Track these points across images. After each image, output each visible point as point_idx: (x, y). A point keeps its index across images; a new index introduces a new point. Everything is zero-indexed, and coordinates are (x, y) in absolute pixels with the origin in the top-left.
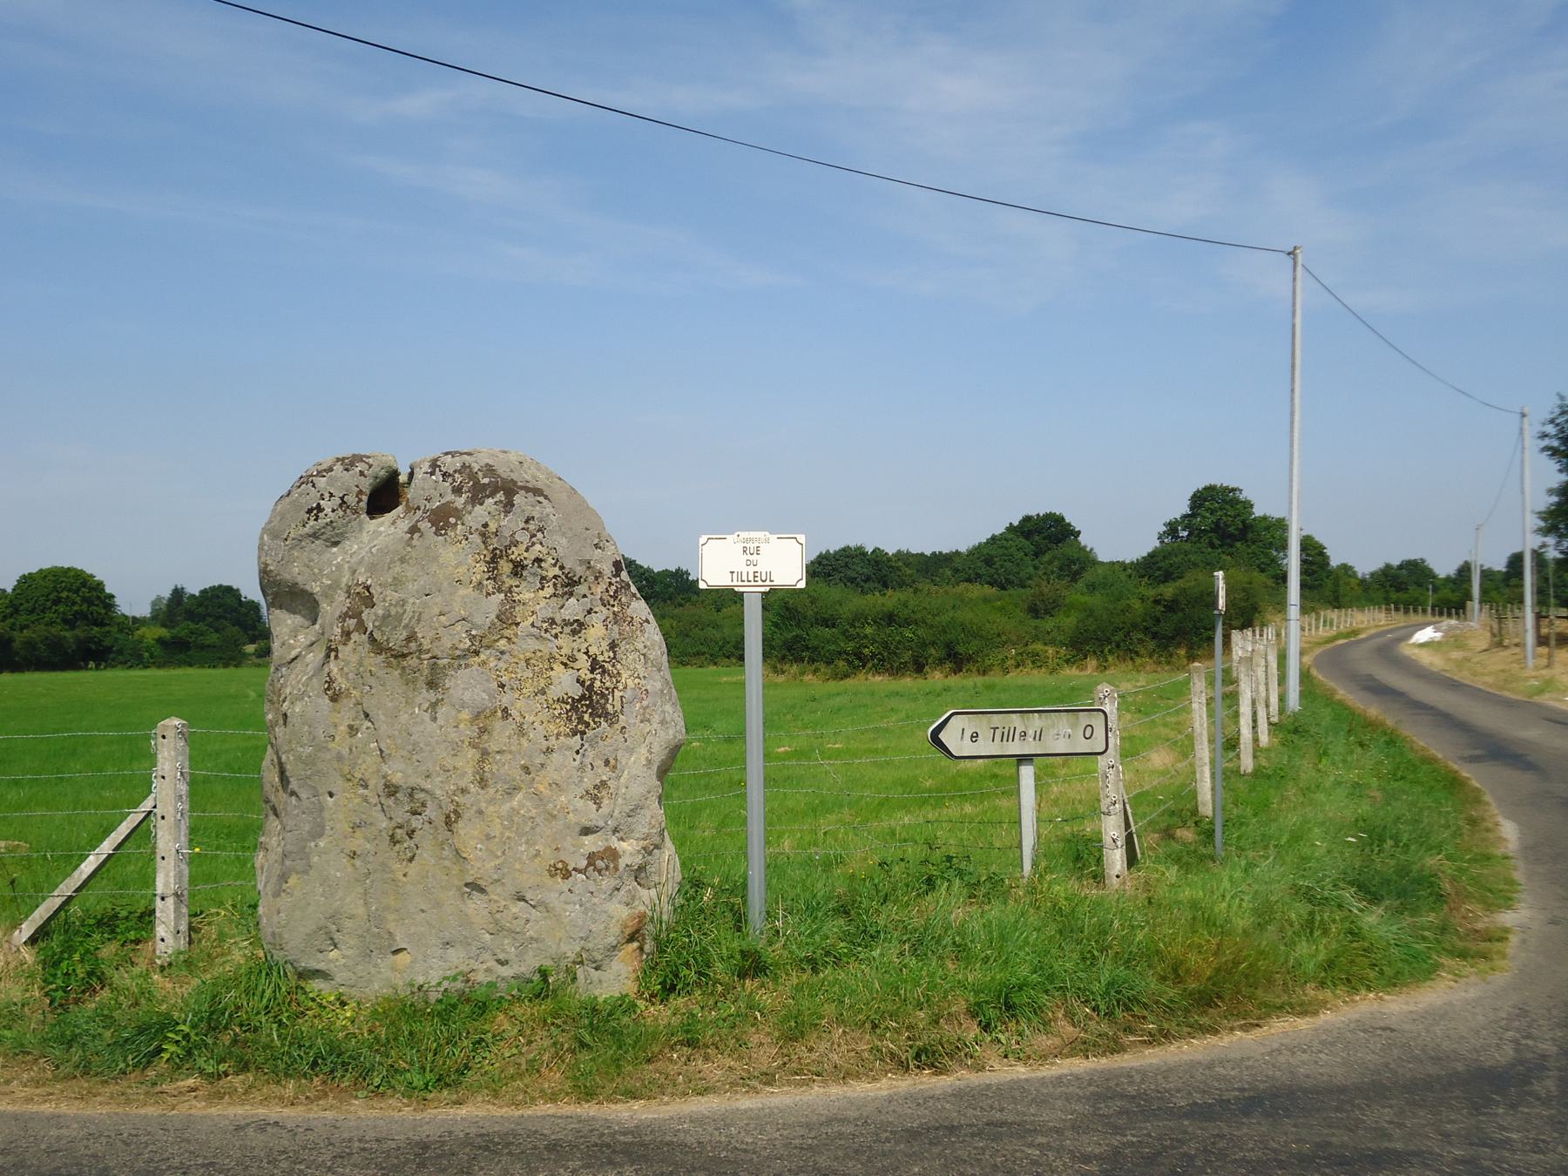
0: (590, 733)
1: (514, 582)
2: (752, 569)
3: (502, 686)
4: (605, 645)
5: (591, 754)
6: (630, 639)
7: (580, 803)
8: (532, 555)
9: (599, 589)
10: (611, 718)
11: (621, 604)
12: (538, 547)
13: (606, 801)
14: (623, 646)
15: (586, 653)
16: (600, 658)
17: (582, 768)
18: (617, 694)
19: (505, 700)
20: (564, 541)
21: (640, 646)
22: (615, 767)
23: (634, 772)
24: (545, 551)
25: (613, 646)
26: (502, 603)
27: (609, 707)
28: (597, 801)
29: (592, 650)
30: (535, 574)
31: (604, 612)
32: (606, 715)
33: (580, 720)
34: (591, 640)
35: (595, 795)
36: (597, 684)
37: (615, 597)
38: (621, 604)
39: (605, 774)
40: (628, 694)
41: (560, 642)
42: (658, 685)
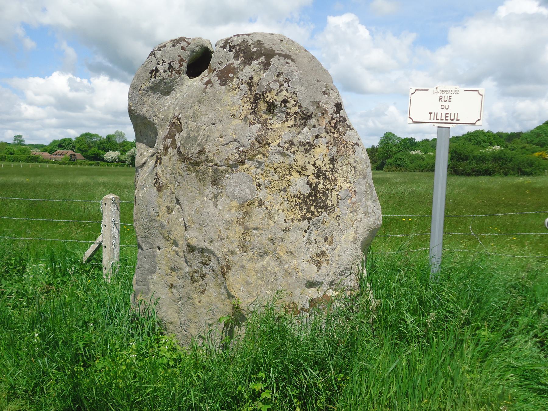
0: (314, 219)
1: (269, 117)
2: (444, 111)
3: (259, 185)
6: (343, 156)
7: (306, 266)
8: (280, 98)
9: (324, 122)
10: (329, 210)
13: (324, 265)
14: (340, 161)
15: (314, 165)
16: (323, 169)
17: (309, 242)
21: (352, 161)
22: (331, 242)
23: (344, 246)
25: (333, 161)
27: (328, 202)
28: (318, 265)
29: (318, 163)
30: (282, 112)
31: (327, 137)
32: (326, 207)
33: (308, 210)
34: (317, 156)
35: (318, 260)
36: (321, 186)
37: (335, 127)
39: (324, 247)
40: (342, 194)
41: (297, 157)
42: (364, 188)
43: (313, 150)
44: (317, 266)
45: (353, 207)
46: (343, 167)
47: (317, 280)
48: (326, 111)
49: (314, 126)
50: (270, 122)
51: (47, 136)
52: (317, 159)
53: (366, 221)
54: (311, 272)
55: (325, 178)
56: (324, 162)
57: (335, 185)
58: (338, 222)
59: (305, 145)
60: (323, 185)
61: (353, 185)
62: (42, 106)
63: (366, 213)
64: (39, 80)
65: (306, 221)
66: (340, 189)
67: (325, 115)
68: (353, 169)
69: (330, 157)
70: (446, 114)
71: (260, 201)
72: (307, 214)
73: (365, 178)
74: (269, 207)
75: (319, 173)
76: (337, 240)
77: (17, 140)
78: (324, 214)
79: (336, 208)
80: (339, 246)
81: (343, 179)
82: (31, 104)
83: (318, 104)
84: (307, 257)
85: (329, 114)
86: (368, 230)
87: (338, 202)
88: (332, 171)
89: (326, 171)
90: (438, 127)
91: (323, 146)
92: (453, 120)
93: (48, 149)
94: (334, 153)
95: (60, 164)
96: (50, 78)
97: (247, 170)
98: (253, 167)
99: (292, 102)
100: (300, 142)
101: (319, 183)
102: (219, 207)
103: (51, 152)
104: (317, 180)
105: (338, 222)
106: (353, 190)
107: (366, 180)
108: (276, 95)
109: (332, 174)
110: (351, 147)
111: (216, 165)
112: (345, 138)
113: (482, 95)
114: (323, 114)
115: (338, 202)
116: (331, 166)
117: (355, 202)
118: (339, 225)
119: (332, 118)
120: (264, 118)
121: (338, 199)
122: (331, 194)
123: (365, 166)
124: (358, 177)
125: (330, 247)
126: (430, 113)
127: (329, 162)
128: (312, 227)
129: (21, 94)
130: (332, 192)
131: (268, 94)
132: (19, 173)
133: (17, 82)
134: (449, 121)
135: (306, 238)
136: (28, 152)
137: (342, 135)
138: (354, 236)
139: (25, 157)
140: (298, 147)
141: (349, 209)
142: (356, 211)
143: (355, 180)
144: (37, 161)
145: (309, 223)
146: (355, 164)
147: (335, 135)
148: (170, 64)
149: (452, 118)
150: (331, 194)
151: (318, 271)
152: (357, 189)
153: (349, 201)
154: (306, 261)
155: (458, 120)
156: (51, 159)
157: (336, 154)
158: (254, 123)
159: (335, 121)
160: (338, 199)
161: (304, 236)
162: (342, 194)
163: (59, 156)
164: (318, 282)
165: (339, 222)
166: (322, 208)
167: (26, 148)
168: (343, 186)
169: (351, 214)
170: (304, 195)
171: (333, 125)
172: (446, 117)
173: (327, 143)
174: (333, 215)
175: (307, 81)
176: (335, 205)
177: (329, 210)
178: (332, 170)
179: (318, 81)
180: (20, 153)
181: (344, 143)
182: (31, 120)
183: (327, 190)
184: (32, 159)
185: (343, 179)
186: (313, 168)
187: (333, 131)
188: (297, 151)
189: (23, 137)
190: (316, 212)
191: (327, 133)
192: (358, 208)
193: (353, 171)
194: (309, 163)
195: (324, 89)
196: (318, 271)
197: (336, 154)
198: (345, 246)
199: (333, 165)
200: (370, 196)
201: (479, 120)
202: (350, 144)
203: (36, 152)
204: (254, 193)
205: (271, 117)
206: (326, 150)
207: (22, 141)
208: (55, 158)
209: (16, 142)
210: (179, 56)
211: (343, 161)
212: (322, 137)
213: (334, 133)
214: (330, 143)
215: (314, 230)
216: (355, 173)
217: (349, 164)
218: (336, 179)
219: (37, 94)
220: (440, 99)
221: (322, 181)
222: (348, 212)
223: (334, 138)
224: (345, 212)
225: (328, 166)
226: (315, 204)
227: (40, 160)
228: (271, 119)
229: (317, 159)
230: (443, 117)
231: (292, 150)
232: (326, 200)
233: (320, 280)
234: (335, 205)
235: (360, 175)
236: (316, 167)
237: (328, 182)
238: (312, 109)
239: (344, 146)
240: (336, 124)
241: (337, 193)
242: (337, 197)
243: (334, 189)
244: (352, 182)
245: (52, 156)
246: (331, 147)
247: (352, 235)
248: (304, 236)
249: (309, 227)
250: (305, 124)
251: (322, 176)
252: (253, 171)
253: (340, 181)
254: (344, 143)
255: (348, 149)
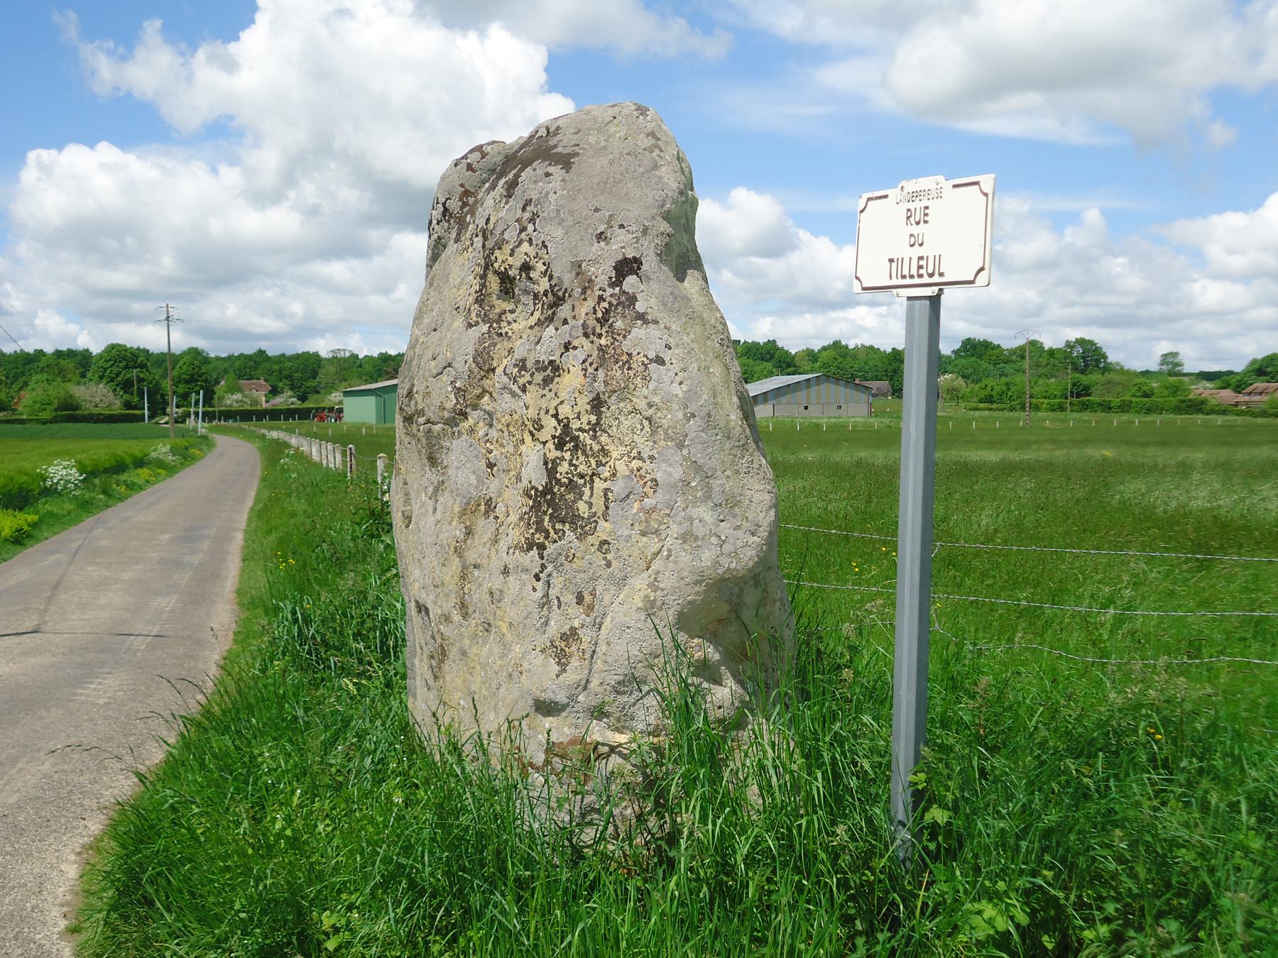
0: (551, 549)
1: (507, 306)
2: (917, 251)
3: (491, 465)
4: (583, 403)
5: (557, 581)
6: (623, 392)
7: (537, 659)
8: (517, 262)
9: (584, 309)
10: (584, 527)
11: (612, 332)
12: (526, 245)
13: (574, 662)
14: (613, 404)
15: (556, 416)
16: (575, 425)
17: (545, 602)
18: (599, 485)
19: (493, 486)
20: (559, 233)
21: (641, 404)
22: (591, 607)
23: (620, 618)
24: (532, 251)
25: (597, 404)
26: (481, 340)
27: (582, 507)
28: (562, 659)
29: (565, 411)
30: (526, 292)
31: (585, 347)
32: (573, 519)
33: (540, 528)
34: (563, 395)
35: (562, 648)
36: (564, 468)
37: (603, 321)
38: (612, 332)
39: (577, 617)
40: (618, 488)
41: (528, 398)
42: (677, 473)
43: (557, 379)
44: (558, 663)
45: (647, 521)
46: (622, 419)
47: (552, 697)
48: (590, 281)
49: (565, 322)
50: (510, 317)
51: (1240, 353)
52: (562, 402)
53: (685, 558)
54: (545, 677)
55: (576, 447)
56: (577, 409)
57: (599, 464)
58: (605, 559)
59: (545, 369)
60: (571, 464)
61: (648, 466)
62: (1244, 278)
63: (685, 537)
64: (1234, 219)
65: (535, 551)
66: (614, 475)
67: (589, 292)
68: (646, 423)
69: (591, 396)
70: (921, 258)
71: (489, 502)
72: (537, 536)
73: (680, 446)
74: (501, 516)
75: (565, 438)
76: (606, 601)
77: (1168, 363)
78: (570, 535)
79: (602, 523)
80: (608, 619)
81: (622, 449)
82: (1218, 276)
83: (580, 266)
84: (543, 640)
85: (597, 288)
86: (697, 583)
87: (607, 508)
88: (595, 431)
89: (580, 429)
90: (909, 298)
91: (576, 370)
92: (931, 275)
93: (1233, 381)
94: (599, 386)
95: (1255, 415)
96: (1260, 211)
97: (472, 431)
98: (481, 424)
99: (540, 267)
100: (538, 362)
101: (563, 459)
102: (439, 515)
103: (1238, 389)
104: (559, 454)
105: (605, 559)
106: (649, 477)
107: (685, 451)
108: (511, 255)
109: (594, 438)
110: (641, 368)
111: (428, 421)
112: (626, 345)
113: (986, 195)
114: (584, 291)
115: (607, 508)
116: (593, 418)
117: (654, 509)
118: (609, 565)
119: (601, 298)
120: (498, 310)
121: (607, 499)
122: (592, 488)
123: (680, 415)
124: (662, 443)
125: (588, 620)
126: (891, 261)
127: (589, 407)
128: (550, 568)
129: (1196, 257)
130: (592, 481)
131: (497, 253)
132: (1107, 441)
133: (1188, 229)
134: (926, 280)
135: (539, 594)
136: (1184, 390)
137: (620, 338)
138: (647, 596)
139: (1174, 400)
140: (532, 375)
141: (637, 527)
142: (656, 532)
143: (654, 453)
144: (1200, 411)
145: (542, 558)
146: (651, 411)
147: (603, 341)
148: (444, 204)
149: (930, 271)
150: (592, 488)
151: (558, 676)
152: (659, 476)
153: (636, 505)
154: (539, 649)
155: (941, 275)
156: (1237, 404)
157: (602, 388)
158: (477, 324)
159: (606, 305)
160: (607, 499)
161: (534, 589)
162: (618, 488)
163: (1258, 398)
164: (556, 703)
165: (609, 557)
166: (564, 523)
167: (1181, 382)
168: (621, 467)
169: (645, 539)
170: (537, 490)
171: (600, 315)
172: (920, 267)
173: (584, 362)
174: (590, 539)
175: (571, 213)
176: (599, 514)
177: (582, 528)
178: (595, 428)
179: (597, 210)
180: (1166, 393)
181: (625, 358)
182: (1215, 315)
183: (582, 476)
184: (1189, 407)
185: (622, 449)
186: (554, 422)
187: (598, 330)
188: (530, 383)
189: (1180, 357)
190: (552, 531)
191: (586, 335)
192: (661, 523)
193: (647, 429)
194: (547, 412)
195: (602, 228)
196: (558, 676)
197: (602, 388)
198: (623, 618)
199: (599, 415)
200: (699, 494)
201: (982, 269)
202: (638, 360)
203: (1204, 390)
204: (483, 483)
205: (512, 306)
206: (581, 379)
207: (1177, 365)
208: (1246, 403)
209: (1165, 367)
210: (462, 185)
211: (622, 405)
212: (575, 348)
213: (600, 336)
214: (590, 360)
215: (555, 574)
216: (653, 433)
217: (635, 411)
218: (603, 449)
219: (1231, 252)
220: (908, 218)
221: (567, 456)
222: (635, 533)
223: (600, 348)
224: (626, 532)
225: (585, 419)
226: (550, 511)
227: (1208, 408)
228: (512, 312)
229: (562, 402)
230: (914, 272)
231: (521, 381)
232: (574, 502)
233: (561, 698)
234: (599, 514)
235: (667, 437)
236: (559, 422)
237: (582, 458)
238: (568, 279)
239: (621, 368)
240: (607, 311)
241: (605, 485)
242: (606, 495)
243: (598, 475)
244: (645, 456)
245: (1242, 398)
246: (590, 370)
247: (642, 594)
248: (534, 589)
249: (543, 567)
250: (550, 319)
251: (569, 442)
252: (481, 433)
253: (615, 454)
254: (625, 358)
255: (631, 373)
